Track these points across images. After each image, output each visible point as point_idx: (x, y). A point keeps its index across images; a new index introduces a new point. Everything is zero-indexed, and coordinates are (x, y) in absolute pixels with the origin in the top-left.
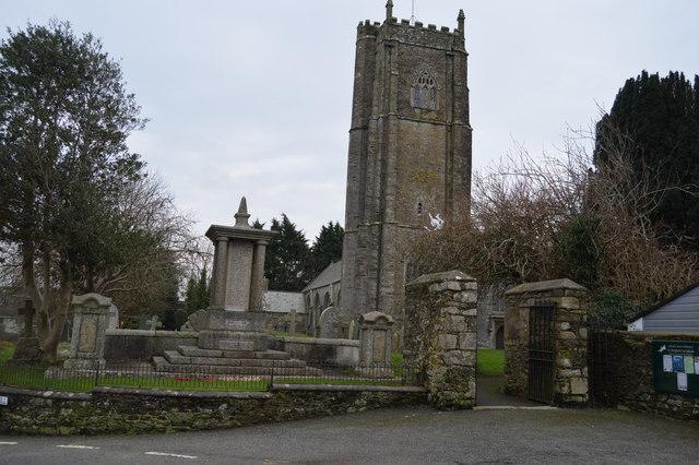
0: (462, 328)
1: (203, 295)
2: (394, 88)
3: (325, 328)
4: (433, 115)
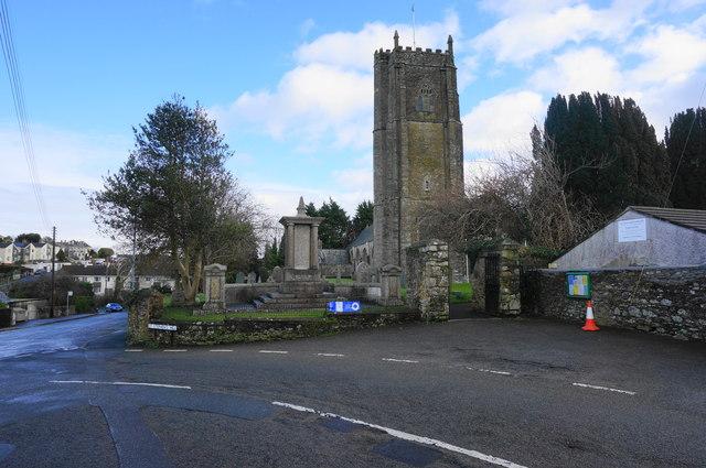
0: (439, 273)
1: (279, 257)
2: (403, 99)
3: (359, 276)
4: (433, 116)
